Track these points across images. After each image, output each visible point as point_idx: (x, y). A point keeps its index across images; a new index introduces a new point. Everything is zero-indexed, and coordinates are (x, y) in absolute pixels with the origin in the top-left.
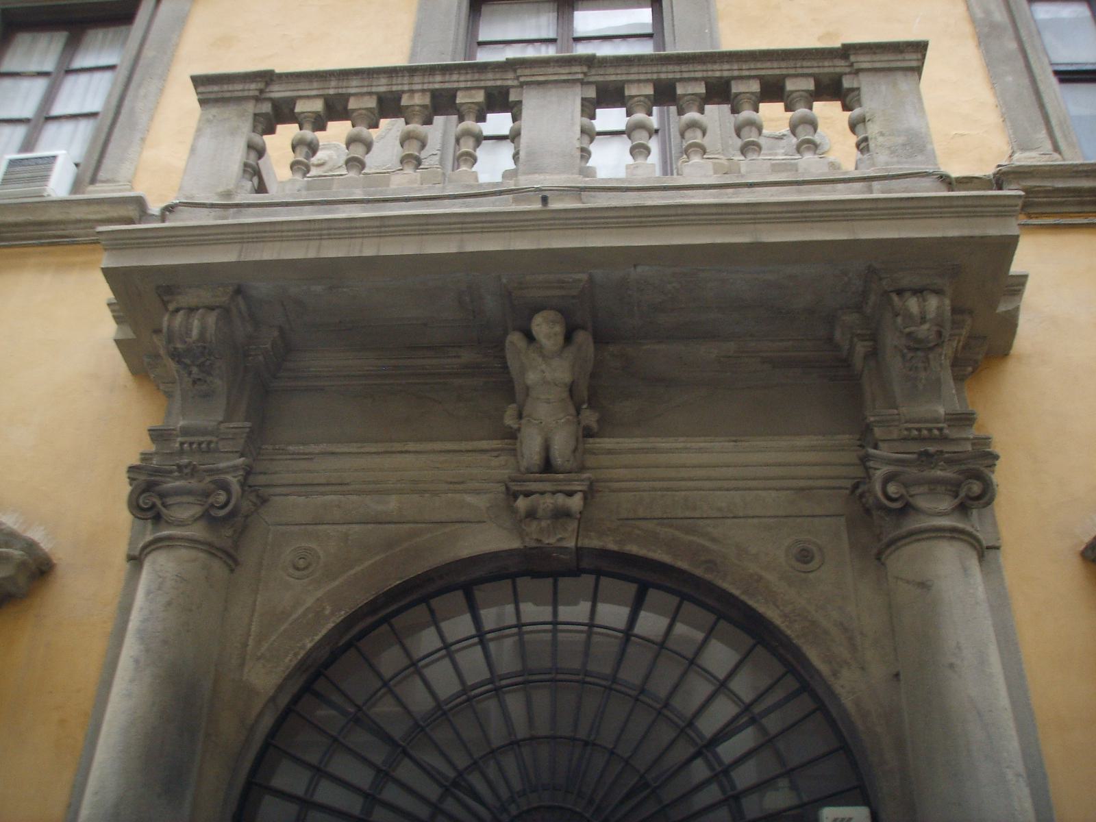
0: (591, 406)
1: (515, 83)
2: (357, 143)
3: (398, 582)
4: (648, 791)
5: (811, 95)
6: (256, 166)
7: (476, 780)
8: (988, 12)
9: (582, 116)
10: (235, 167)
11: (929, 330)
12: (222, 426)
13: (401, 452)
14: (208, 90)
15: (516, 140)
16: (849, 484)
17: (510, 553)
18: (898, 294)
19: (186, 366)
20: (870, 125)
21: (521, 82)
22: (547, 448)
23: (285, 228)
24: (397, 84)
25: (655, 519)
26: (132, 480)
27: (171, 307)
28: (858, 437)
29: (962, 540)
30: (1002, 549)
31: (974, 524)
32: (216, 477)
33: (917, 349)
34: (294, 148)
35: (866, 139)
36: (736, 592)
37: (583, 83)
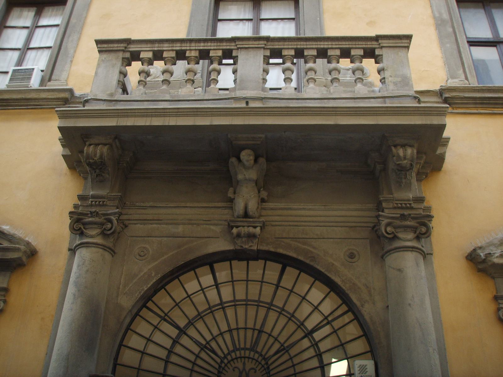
0: (264, 190)
1: (235, 47)
3: (183, 263)
4: (285, 350)
7: (213, 344)
8: (440, 14)
9: (264, 64)
10: (115, 82)
11: (407, 163)
12: (109, 194)
13: (184, 207)
16: (372, 225)
17: (229, 251)
18: (394, 147)
19: (94, 169)
20: (386, 72)
21: (238, 48)
22: (246, 208)
23: (136, 111)
25: (290, 238)
26: (71, 217)
27: (87, 143)
28: (376, 205)
29: (416, 251)
30: (433, 255)
31: (422, 244)
32: (107, 217)
33: (402, 170)
34: (140, 74)
35: (384, 78)
36: (323, 271)
37: (264, 48)
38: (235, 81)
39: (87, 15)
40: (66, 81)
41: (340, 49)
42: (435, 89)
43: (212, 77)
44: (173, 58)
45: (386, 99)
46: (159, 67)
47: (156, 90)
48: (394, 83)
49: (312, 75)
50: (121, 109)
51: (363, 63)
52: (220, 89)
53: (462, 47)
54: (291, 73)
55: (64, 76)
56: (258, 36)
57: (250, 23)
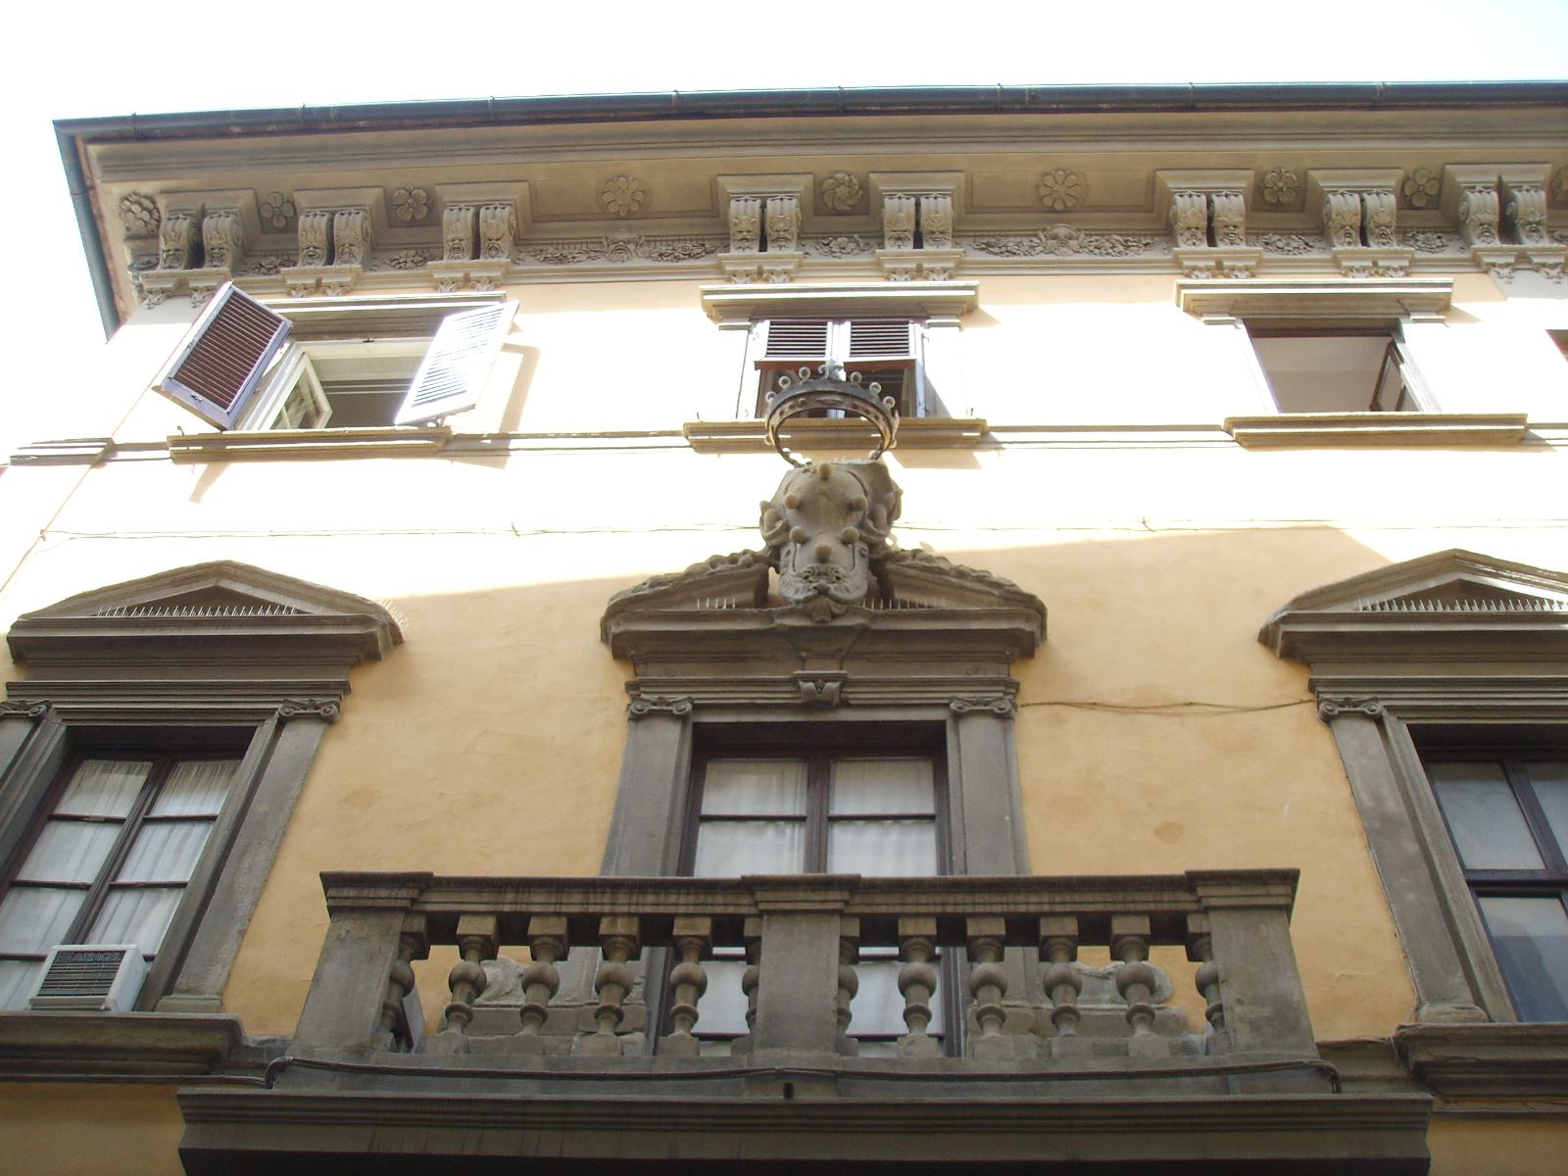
1: (753, 910)
2: (540, 985)
5: (1145, 940)
6: (399, 1007)
8: (1378, 798)
10: (373, 1011)
14: (340, 895)
15: (752, 993)
20: (1224, 988)
24: (595, 904)
34: (452, 985)
35: (1219, 1008)
37: (842, 914)
38: (751, 1017)
39: (302, 791)
40: (220, 994)
41: (1079, 915)
42: (1382, 1036)
43: (680, 1003)
44: (558, 937)
45: (1230, 1077)
46: (513, 962)
47: (499, 1037)
48: (1251, 1023)
49: (993, 1002)
50: (386, 1100)
51: (1150, 957)
52: (703, 1037)
53: (1455, 902)
54: (926, 992)
55: (215, 976)
56: (822, 874)
57: (797, 829)
